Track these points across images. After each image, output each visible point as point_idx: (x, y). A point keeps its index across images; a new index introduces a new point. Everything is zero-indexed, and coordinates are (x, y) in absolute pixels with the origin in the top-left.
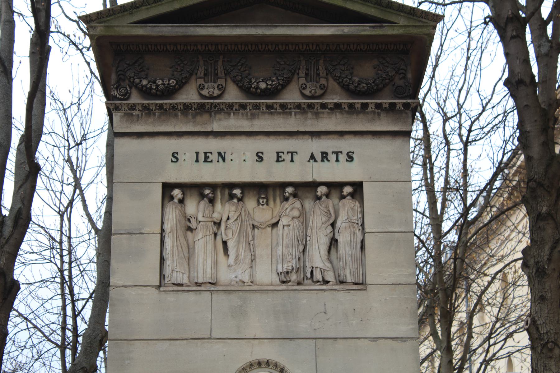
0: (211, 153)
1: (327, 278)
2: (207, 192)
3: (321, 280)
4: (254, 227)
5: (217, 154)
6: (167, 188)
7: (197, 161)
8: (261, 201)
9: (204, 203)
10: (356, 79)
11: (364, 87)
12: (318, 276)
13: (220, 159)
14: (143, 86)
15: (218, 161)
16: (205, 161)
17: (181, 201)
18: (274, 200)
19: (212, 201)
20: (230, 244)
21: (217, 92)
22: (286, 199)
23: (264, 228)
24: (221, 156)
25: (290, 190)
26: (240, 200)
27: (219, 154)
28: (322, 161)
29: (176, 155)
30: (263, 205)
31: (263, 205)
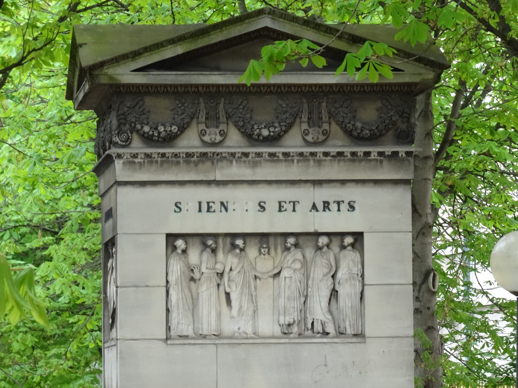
0: (214, 203)
1: (328, 330)
2: (210, 242)
3: (321, 331)
4: (256, 277)
5: (219, 204)
6: (171, 238)
7: (200, 211)
8: (262, 250)
9: (207, 255)
10: (359, 125)
11: (367, 134)
12: (318, 327)
13: (223, 209)
14: (144, 133)
15: (221, 211)
17: (184, 251)
18: (276, 249)
19: (214, 251)
20: (233, 296)
21: (219, 138)
22: (288, 249)
23: (267, 279)
25: (291, 240)
26: (242, 250)
27: (222, 204)
28: (324, 210)
29: (179, 205)
30: (264, 255)
31: (264, 255)
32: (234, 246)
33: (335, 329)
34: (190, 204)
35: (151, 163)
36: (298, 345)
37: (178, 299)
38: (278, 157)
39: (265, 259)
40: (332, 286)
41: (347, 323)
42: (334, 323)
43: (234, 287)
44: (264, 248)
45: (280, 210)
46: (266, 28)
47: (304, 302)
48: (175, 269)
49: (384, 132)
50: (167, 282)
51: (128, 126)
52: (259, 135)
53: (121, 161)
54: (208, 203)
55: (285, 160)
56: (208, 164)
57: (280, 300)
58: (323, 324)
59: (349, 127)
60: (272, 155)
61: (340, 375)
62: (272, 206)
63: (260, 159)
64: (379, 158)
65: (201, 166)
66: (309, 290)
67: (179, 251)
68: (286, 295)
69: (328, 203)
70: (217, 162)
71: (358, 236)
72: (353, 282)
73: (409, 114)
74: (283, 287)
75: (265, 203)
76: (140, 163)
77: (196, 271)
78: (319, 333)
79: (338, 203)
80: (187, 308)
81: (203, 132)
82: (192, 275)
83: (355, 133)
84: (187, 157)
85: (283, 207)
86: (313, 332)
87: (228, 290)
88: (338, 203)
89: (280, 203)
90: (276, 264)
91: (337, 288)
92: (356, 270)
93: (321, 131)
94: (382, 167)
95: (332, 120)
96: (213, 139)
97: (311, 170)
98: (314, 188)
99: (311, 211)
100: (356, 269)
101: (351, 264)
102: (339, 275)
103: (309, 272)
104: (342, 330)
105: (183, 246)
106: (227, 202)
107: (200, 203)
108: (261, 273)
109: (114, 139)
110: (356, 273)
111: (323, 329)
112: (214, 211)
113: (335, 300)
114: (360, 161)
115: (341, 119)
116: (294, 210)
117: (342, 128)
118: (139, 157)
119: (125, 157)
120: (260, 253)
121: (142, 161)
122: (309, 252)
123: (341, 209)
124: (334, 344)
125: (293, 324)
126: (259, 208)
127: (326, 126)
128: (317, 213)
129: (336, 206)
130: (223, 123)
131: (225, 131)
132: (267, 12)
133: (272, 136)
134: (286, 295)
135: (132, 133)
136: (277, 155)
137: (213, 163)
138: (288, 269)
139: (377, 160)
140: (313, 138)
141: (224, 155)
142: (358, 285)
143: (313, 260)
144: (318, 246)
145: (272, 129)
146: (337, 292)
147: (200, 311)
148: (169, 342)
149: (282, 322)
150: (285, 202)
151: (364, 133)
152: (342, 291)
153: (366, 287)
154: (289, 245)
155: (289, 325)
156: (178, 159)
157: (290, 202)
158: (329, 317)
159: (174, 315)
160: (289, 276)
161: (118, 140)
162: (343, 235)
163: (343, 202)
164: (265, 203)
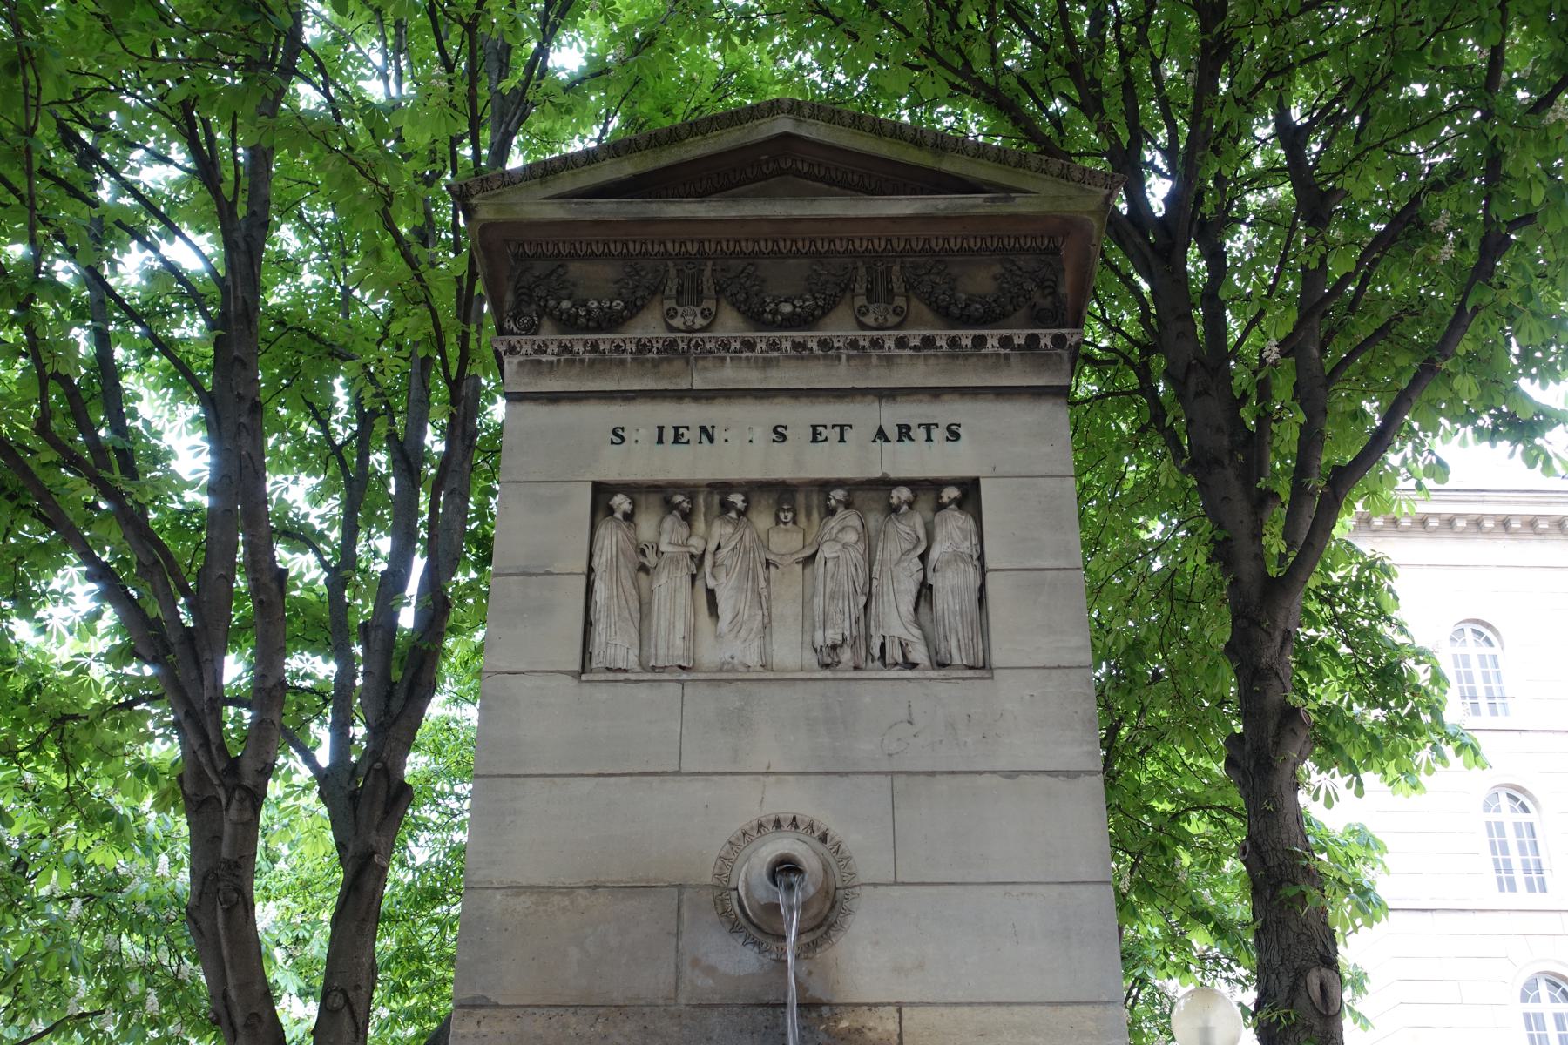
0: (687, 428)
4: (768, 564)
6: (602, 492)
7: (660, 441)
8: (782, 516)
11: (977, 310)
12: (894, 653)
13: (704, 438)
14: (562, 313)
16: (676, 441)
17: (629, 517)
18: (809, 516)
19: (687, 517)
24: (707, 433)
27: (703, 429)
28: (900, 440)
29: (620, 432)
30: (785, 523)
31: (785, 523)
32: (726, 506)
33: (930, 658)
34: (641, 431)
35: (570, 363)
36: (853, 683)
37: (609, 598)
38: (811, 349)
39: (787, 530)
40: (921, 575)
41: (954, 643)
42: (927, 646)
43: (723, 579)
44: (784, 510)
45: (814, 440)
46: (786, 136)
47: (866, 607)
48: (607, 542)
49: (1010, 307)
50: (591, 570)
51: (534, 307)
52: (775, 312)
53: (516, 360)
54: (676, 429)
55: (825, 357)
56: (678, 364)
57: (816, 600)
58: (903, 647)
59: (944, 300)
60: (798, 346)
61: (941, 741)
62: (799, 434)
63: (775, 354)
64: (1002, 351)
65: (665, 367)
66: (875, 582)
67: (618, 515)
68: (828, 590)
69: (908, 428)
70: (696, 359)
71: (969, 493)
72: (961, 565)
73: (1055, 283)
74: (821, 578)
75: (785, 428)
76: (552, 362)
77: (650, 553)
78: (896, 664)
79: (928, 427)
80: (626, 614)
81: (672, 312)
82: (642, 559)
83: (955, 310)
84: (639, 351)
85: (820, 434)
86: (885, 665)
87: (711, 584)
88: (928, 427)
89: (814, 427)
90: (809, 540)
91: (930, 581)
92: (967, 546)
93: (890, 308)
94: (1009, 366)
95: (911, 293)
96: (689, 323)
97: (874, 372)
98: (880, 403)
99: (874, 441)
100: (967, 543)
101: (957, 536)
102: (935, 554)
103: (873, 543)
104: (943, 657)
105: (626, 506)
106: (713, 427)
107: (661, 429)
108: (777, 554)
109: (506, 325)
110: (969, 551)
111: (904, 655)
112: (688, 442)
113: (928, 606)
114: (967, 357)
115: (928, 289)
116: (842, 440)
117: (929, 306)
118: (549, 351)
119: (523, 352)
120: (778, 521)
121: (554, 358)
122: (874, 520)
123: (933, 436)
124: (925, 682)
125: (841, 646)
126: (774, 436)
127: (900, 301)
128: (885, 445)
129: (922, 433)
130: (710, 298)
131: (714, 310)
132: (786, 106)
133: (799, 316)
134: (828, 590)
135: (540, 317)
136: (810, 345)
137: (688, 362)
138: (830, 543)
139: (998, 355)
140: (876, 319)
141: (708, 346)
142: (972, 575)
143: (882, 531)
144: (891, 505)
145: (798, 303)
146: (931, 587)
147: (654, 622)
148: (584, 677)
149: (819, 642)
150: (825, 427)
151: (972, 308)
152: (940, 582)
153: (989, 575)
154: (833, 502)
155: (834, 647)
156: (623, 356)
157: (833, 426)
158: (917, 632)
159: (600, 628)
160: (835, 555)
161: (512, 325)
162: (937, 485)
163: (937, 425)
164: (785, 428)
